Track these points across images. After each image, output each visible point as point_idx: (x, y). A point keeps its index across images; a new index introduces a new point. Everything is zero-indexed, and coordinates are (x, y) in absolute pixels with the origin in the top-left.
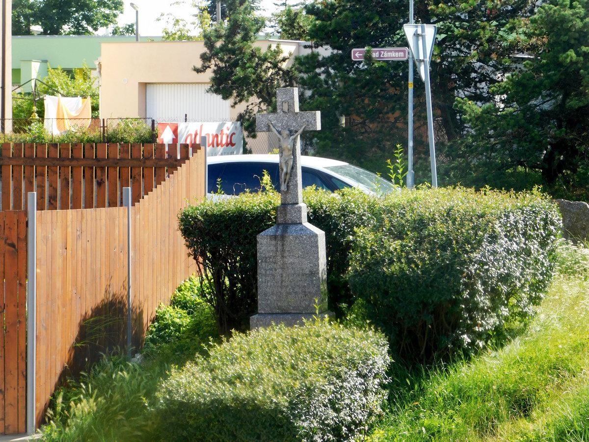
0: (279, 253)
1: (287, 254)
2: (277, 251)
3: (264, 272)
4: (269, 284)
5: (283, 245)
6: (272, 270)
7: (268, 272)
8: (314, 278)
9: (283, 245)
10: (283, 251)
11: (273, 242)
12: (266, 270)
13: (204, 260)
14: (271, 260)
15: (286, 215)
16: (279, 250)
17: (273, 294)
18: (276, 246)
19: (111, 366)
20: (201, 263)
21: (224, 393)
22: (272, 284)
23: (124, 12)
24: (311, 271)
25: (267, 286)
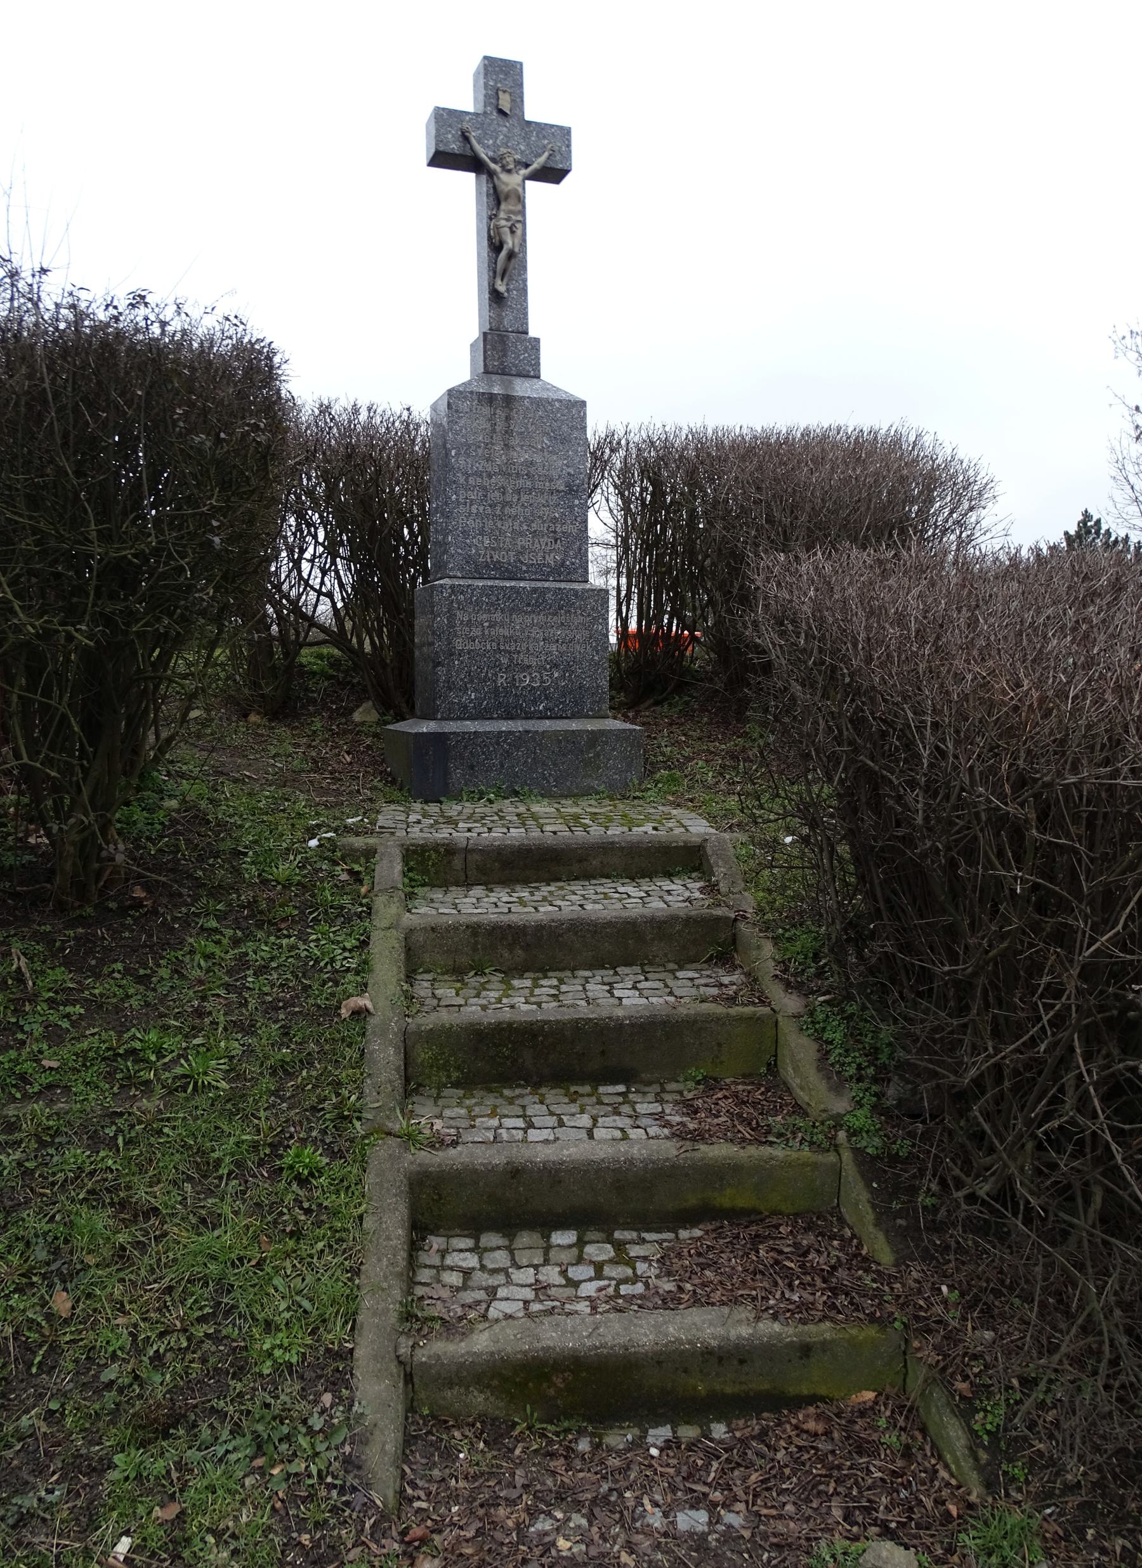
0: (497, 438)
1: (515, 441)
2: (494, 431)
3: (462, 480)
4: (474, 509)
5: (508, 418)
6: (481, 476)
7: (471, 481)
8: (577, 502)
9: (508, 418)
10: (508, 432)
11: (486, 410)
12: (467, 475)
13: (298, 525)
14: (480, 451)
15: (505, 355)
16: (498, 429)
17: (482, 533)
18: (491, 419)
19: (923, 738)
20: (312, 588)
21: (695, 1388)
22: (481, 508)
23: (136, 285)
24: (568, 485)
25: (470, 514)
